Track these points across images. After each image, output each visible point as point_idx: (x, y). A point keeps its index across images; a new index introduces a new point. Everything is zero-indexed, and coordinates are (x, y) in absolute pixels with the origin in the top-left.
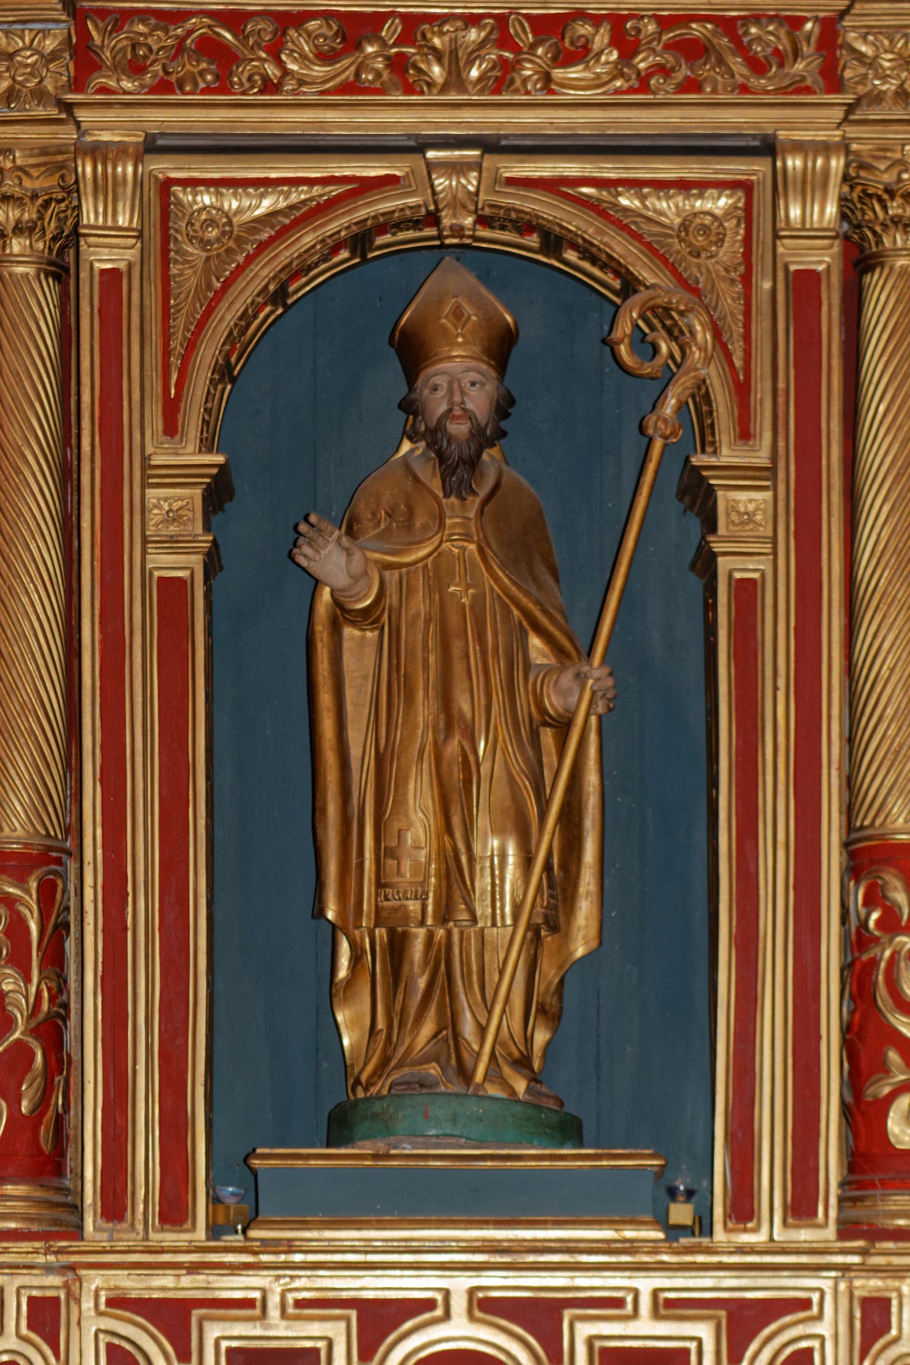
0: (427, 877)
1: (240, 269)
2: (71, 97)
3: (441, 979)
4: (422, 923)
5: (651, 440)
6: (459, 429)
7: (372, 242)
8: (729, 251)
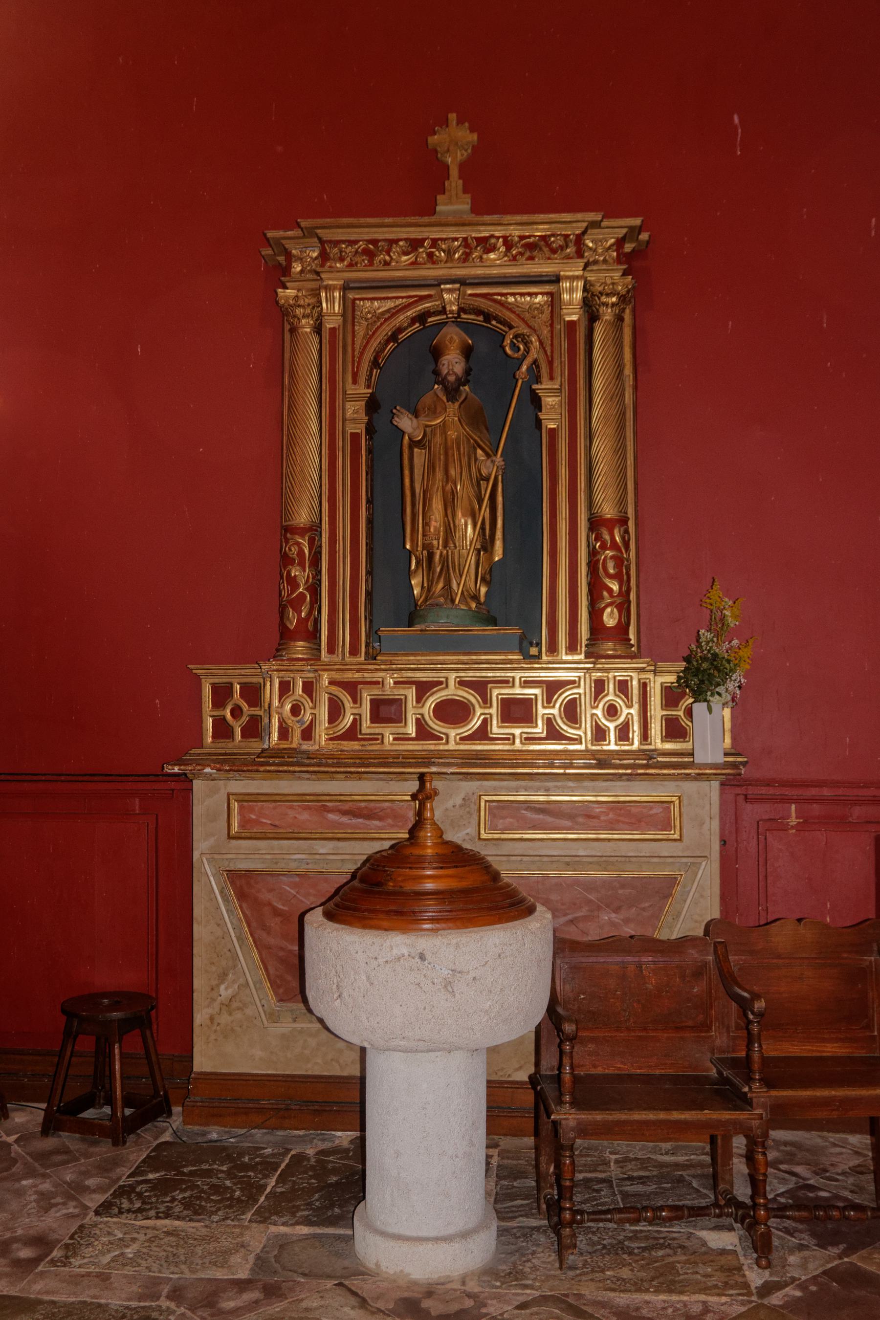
0: (439, 532)
1: (378, 328)
2: (319, 269)
3: (445, 568)
4: (438, 549)
5: (517, 380)
6: (452, 378)
7: (426, 320)
8: (546, 316)
